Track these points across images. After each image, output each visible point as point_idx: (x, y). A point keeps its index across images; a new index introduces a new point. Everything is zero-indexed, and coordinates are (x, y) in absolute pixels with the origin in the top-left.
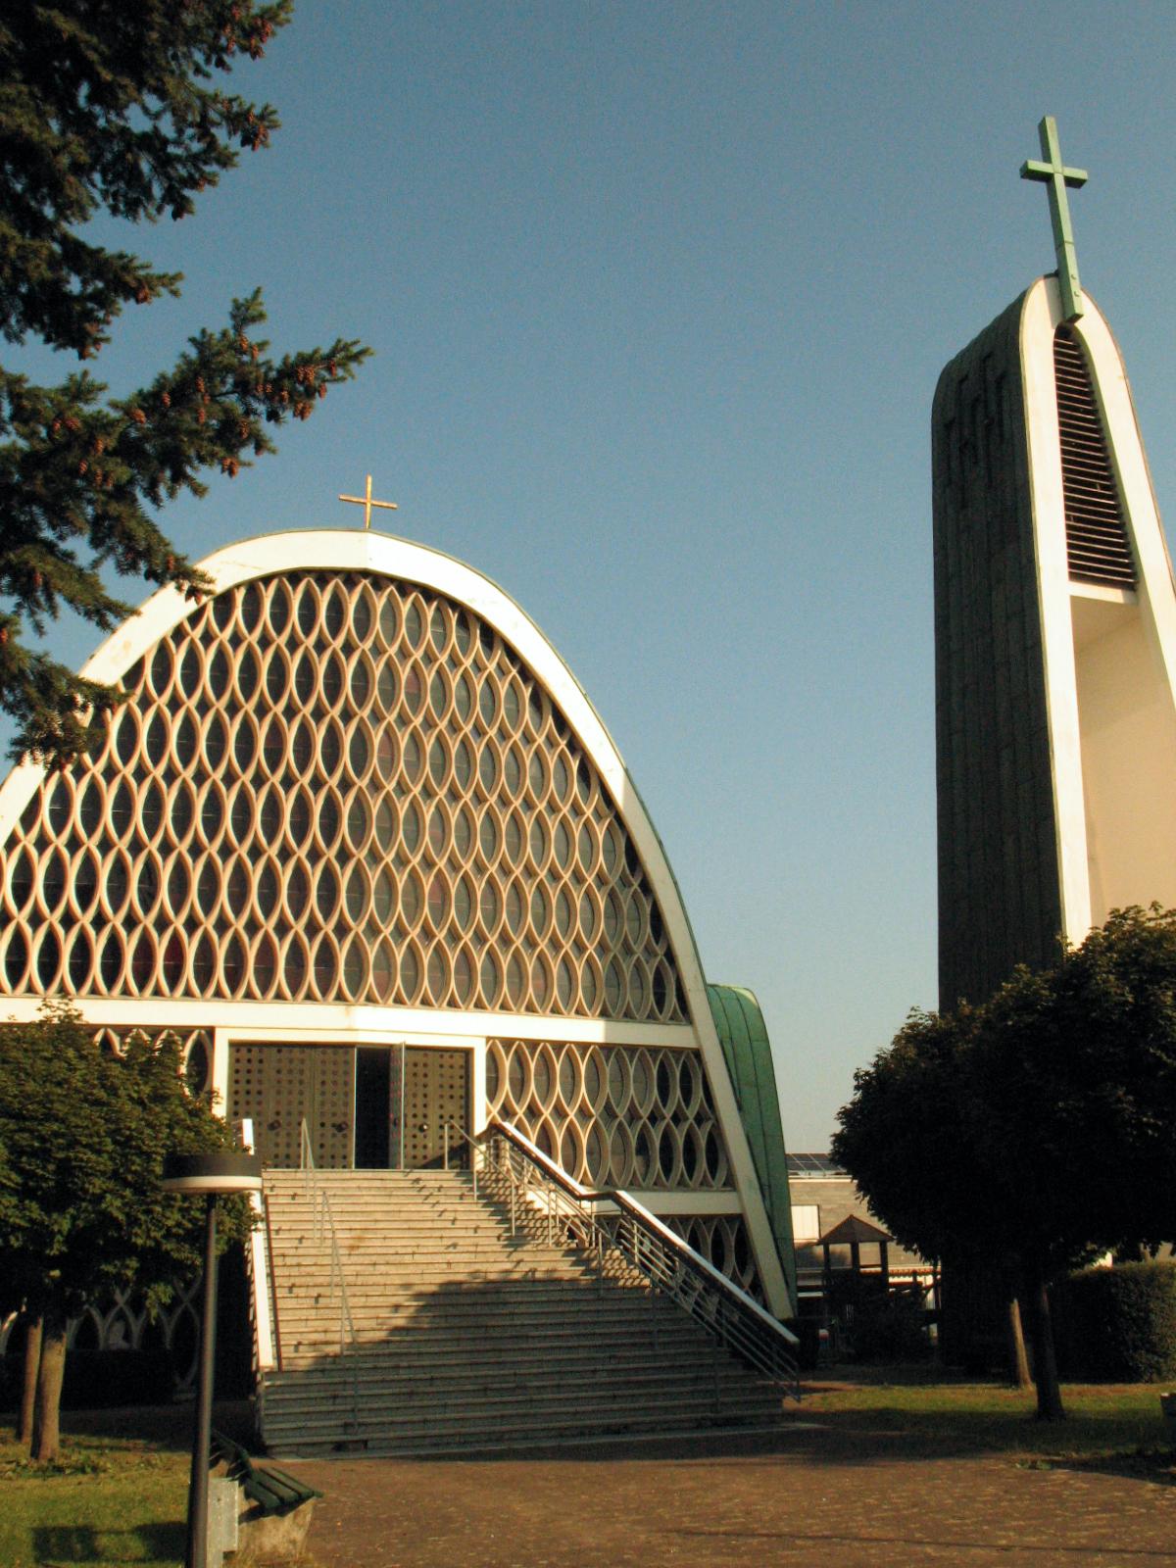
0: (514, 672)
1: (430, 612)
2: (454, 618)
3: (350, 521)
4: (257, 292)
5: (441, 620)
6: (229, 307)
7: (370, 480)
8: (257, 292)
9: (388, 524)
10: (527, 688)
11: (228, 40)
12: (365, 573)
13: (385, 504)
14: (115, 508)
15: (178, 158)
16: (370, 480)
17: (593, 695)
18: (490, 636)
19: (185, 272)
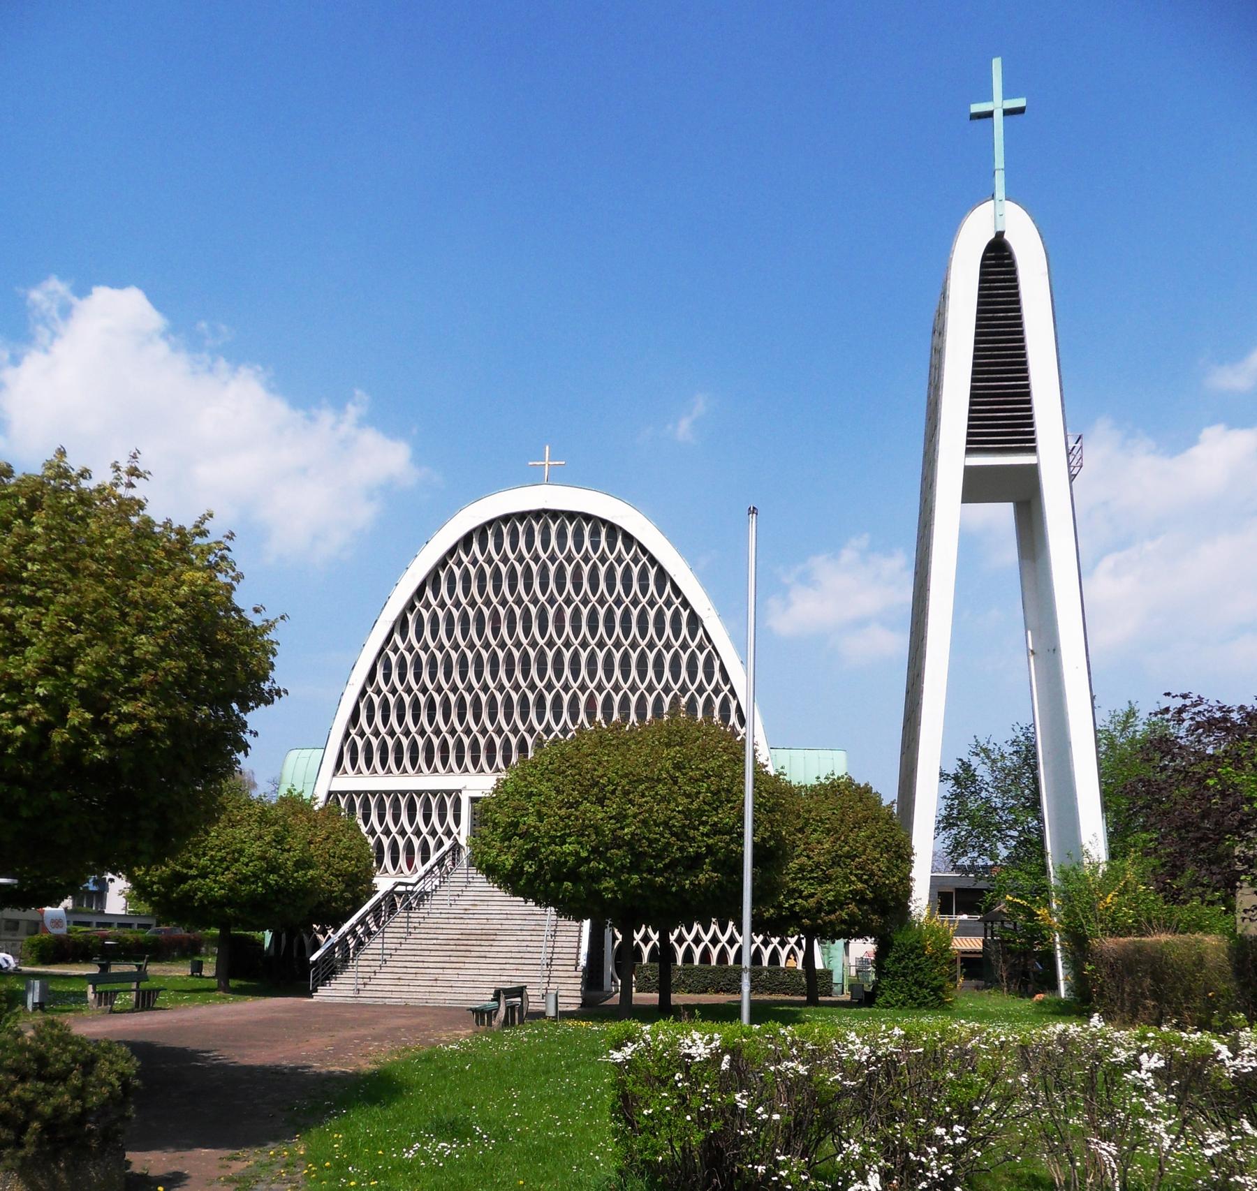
0: (644, 559)
1: (587, 530)
2: (603, 532)
3: (534, 479)
4: (1130, 702)
5: (595, 533)
6: (131, 1160)
7: (547, 448)
8: (1130, 702)
9: (559, 478)
10: (653, 568)
11: (426, 1122)
12: (546, 511)
13: (557, 463)
14: (144, 985)
15: (929, 1178)
16: (547, 448)
17: (665, 529)
18: (629, 539)
19: (999, 229)
